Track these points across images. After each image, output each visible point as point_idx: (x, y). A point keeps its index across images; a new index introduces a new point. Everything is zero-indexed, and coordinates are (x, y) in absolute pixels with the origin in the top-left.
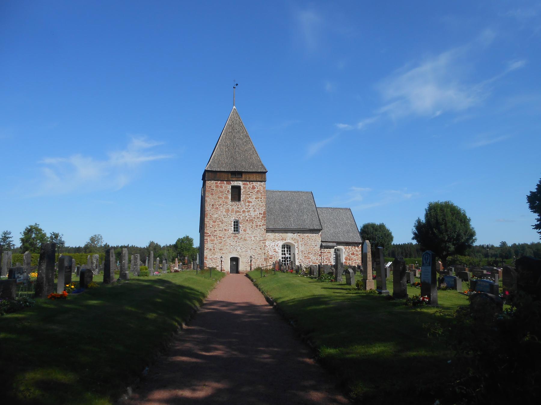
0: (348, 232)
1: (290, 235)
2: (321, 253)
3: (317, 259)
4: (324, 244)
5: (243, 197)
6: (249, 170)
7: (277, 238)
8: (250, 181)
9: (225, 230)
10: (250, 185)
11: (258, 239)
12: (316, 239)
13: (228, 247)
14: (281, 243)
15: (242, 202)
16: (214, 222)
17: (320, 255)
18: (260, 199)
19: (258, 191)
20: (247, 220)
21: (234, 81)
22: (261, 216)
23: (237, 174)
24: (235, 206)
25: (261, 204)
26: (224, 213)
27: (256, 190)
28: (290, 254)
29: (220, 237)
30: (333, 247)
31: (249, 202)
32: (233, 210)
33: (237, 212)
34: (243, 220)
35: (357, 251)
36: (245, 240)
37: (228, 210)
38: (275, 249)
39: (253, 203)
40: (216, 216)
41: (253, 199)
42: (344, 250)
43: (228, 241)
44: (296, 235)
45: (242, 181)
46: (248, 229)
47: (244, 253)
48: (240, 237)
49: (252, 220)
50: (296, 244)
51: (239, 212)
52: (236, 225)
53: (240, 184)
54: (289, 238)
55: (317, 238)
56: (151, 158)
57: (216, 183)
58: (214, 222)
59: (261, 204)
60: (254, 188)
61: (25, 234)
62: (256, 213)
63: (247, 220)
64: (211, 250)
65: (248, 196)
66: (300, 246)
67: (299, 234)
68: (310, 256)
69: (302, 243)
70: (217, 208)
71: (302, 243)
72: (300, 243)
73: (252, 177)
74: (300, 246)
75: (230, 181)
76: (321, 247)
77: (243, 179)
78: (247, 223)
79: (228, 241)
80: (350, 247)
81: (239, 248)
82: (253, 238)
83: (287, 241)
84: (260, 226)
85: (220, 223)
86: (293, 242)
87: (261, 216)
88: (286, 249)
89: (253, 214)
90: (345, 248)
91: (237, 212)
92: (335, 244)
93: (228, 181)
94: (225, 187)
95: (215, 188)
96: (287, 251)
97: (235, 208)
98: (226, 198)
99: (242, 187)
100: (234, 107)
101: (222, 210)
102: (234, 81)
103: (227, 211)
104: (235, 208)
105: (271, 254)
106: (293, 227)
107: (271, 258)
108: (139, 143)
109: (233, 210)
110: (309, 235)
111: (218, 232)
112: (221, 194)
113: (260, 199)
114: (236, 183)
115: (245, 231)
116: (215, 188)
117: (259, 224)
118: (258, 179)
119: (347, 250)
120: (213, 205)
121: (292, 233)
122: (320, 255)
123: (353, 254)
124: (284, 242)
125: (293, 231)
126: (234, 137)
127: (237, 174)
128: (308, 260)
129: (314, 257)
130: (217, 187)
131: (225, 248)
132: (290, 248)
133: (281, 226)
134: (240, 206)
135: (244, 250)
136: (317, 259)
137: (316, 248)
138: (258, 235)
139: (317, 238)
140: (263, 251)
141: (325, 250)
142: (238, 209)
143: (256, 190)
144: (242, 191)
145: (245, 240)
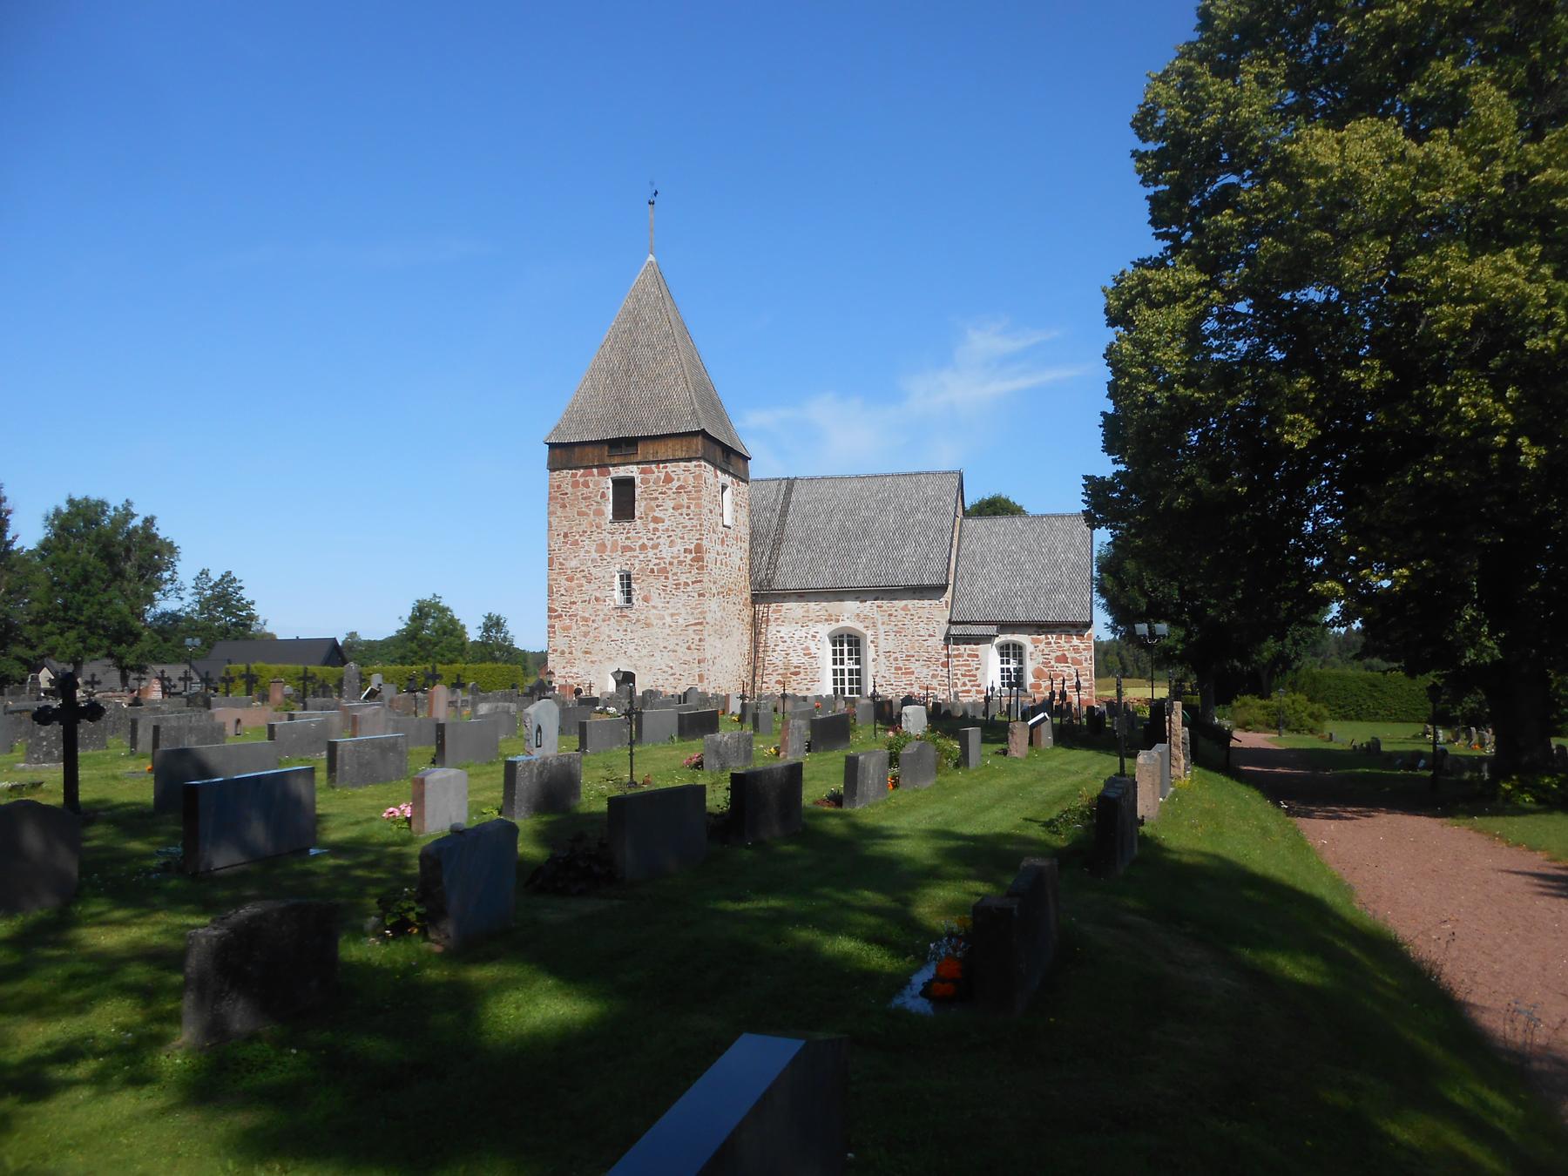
0: (1055, 588)
1: (851, 606)
2: (948, 656)
3: (934, 676)
4: (955, 630)
5: (640, 507)
6: (655, 432)
7: (812, 615)
8: (658, 462)
9: (597, 599)
10: (658, 472)
11: (681, 621)
12: (934, 615)
13: (604, 646)
14: (824, 630)
15: (639, 522)
16: (570, 579)
17: (946, 665)
18: (684, 511)
19: (680, 487)
20: (652, 571)
21: (652, 184)
22: (690, 557)
23: (623, 447)
24: (622, 533)
25: (688, 523)
26: (595, 555)
27: (676, 484)
28: (858, 662)
29: (585, 619)
30: (988, 639)
31: (656, 520)
32: (615, 544)
33: (626, 549)
34: (642, 570)
35: (1076, 650)
36: (648, 625)
37: (604, 545)
38: (808, 648)
39: (667, 523)
40: (574, 563)
41: (666, 513)
42: (1029, 648)
43: (605, 629)
44: (869, 607)
45: (638, 463)
46: (654, 596)
47: (646, 660)
48: (634, 617)
49: (664, 570)
50: (869, 633)
51: (631, 549)
52: (627, 580)
53: (632, 471)
54: (850, 614)
55: (936, 612)
56: (1023, 383)
57: (574, 475)
58: (570, 579)
59: (688, 523)
60: (668, 479)
61: (413, 619)
62: (675, 549)
63: (652, 571)
64: (563, 653)
65: (653, 504)
66: (882, 636)
67: (878, 602)
68: (914, 666)
69: (887, 628)
70: (576, 543)
71: (887, 628)
72: (882, 629)
73: (664, 450)
74: (882, 636)
75: (606, 466)
76: (948, 638)
77: (639, 458)
78: (651, 579)
79: (605, 629)
80: (1052, 638)
81: (632, 647)
82: (668, 620)
83: (841, 624)
84: (686, 584)
85: (584, 581)
86: (859, 627)
87: (690, 557)
88: (846, 647)
89: (667, 553)
90: (1034, 641)
91: (626, 549)
92: (992, 630)
93: (603, 467)
94: (597, 484)
95: (570, 490)
96: (850, 652)
97: (621, 539)
98: (599, 513)
99: (637, 481)
100: (651, 258)
101: (589, 545)
102: (652, 184)
103: (602, 547)
104: (621, 539)
105: (795, 661)
106: (860, 581)
107: (797, 674)
108: (985, 341)
109: (615, 544)
110: (910, 603)
111: (579, 606)
112: (584, 503)
113: (684, 511)
114: (622, 472)
115: (646, 599)
116: (570, 490)
117: (683, 579)
118: (679, 454)
119: (1042, 646)
120: (566, 535)
121: (857, 599)
122: (946, 665)
123: (1062, 659)
124: (835, 626)
125: (860, 594)
126: (635, 343)
127: (623, 447)
128: (905, 679)
129: (925, 671)
130: (575, 484)
131: (596, 647)
132: (857, 643)
133: (824, 580)
134: (633, 534)
135: (644, 652)
136: (934, 676)
137: (932, 641)
138: (683, 611)
139: (936, 612)
140: (696, 655)
141: (962, 647)
142: (628, 543)
143: (676, 484)
144: (638, 491)
145: (648, 625)
